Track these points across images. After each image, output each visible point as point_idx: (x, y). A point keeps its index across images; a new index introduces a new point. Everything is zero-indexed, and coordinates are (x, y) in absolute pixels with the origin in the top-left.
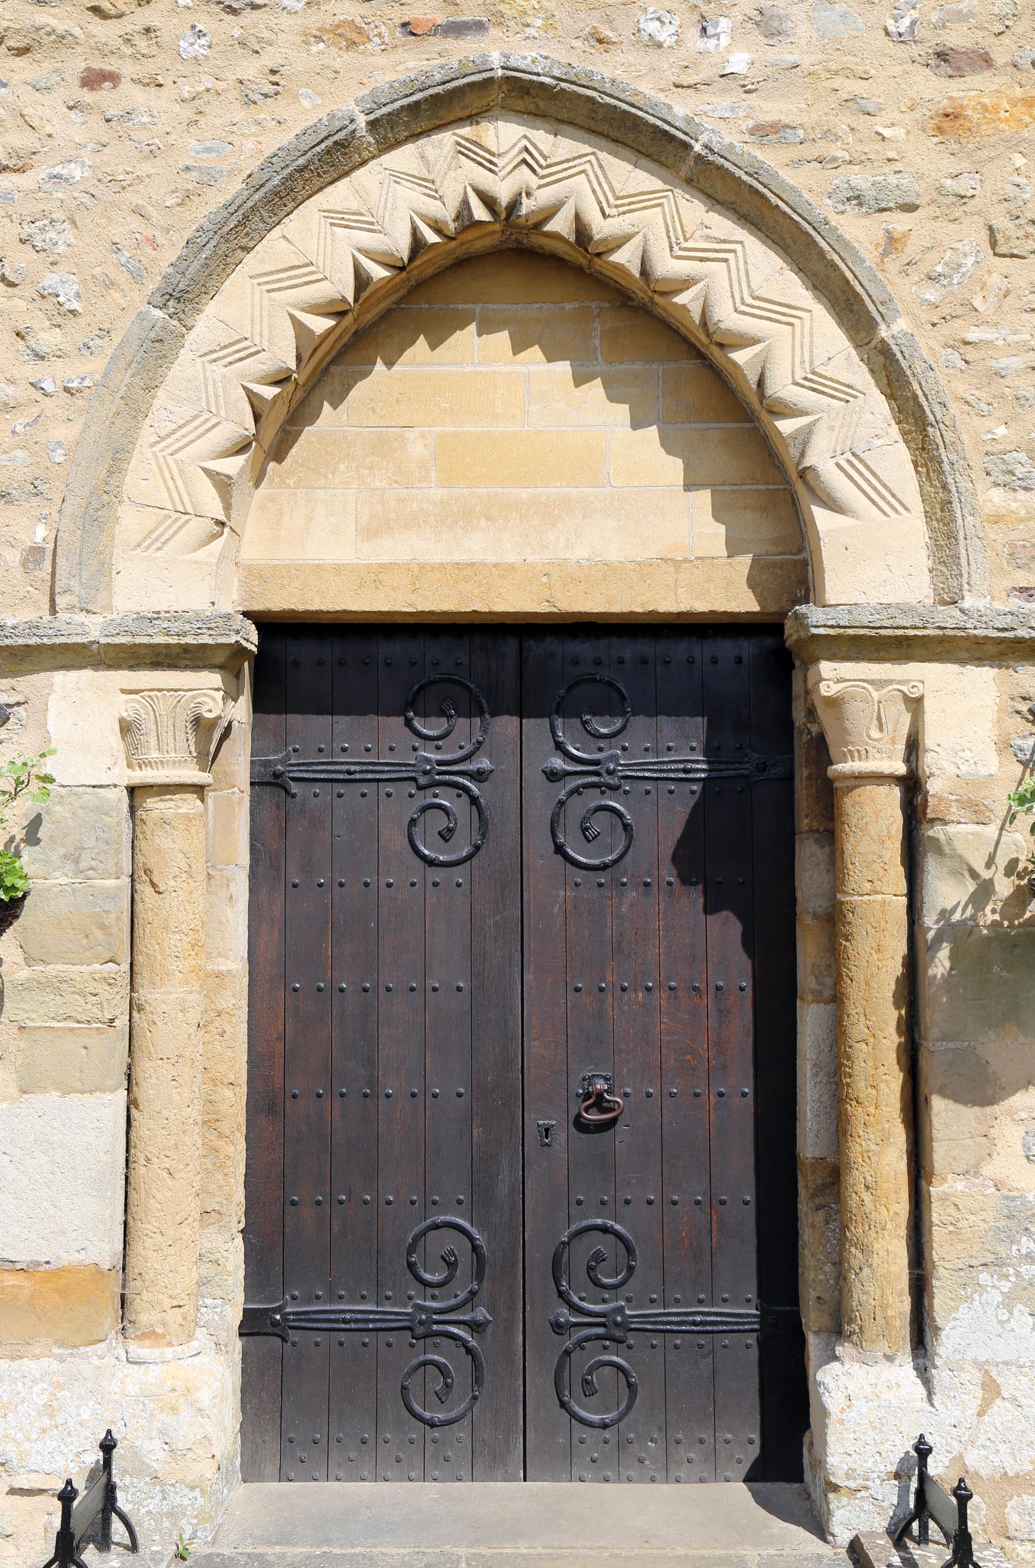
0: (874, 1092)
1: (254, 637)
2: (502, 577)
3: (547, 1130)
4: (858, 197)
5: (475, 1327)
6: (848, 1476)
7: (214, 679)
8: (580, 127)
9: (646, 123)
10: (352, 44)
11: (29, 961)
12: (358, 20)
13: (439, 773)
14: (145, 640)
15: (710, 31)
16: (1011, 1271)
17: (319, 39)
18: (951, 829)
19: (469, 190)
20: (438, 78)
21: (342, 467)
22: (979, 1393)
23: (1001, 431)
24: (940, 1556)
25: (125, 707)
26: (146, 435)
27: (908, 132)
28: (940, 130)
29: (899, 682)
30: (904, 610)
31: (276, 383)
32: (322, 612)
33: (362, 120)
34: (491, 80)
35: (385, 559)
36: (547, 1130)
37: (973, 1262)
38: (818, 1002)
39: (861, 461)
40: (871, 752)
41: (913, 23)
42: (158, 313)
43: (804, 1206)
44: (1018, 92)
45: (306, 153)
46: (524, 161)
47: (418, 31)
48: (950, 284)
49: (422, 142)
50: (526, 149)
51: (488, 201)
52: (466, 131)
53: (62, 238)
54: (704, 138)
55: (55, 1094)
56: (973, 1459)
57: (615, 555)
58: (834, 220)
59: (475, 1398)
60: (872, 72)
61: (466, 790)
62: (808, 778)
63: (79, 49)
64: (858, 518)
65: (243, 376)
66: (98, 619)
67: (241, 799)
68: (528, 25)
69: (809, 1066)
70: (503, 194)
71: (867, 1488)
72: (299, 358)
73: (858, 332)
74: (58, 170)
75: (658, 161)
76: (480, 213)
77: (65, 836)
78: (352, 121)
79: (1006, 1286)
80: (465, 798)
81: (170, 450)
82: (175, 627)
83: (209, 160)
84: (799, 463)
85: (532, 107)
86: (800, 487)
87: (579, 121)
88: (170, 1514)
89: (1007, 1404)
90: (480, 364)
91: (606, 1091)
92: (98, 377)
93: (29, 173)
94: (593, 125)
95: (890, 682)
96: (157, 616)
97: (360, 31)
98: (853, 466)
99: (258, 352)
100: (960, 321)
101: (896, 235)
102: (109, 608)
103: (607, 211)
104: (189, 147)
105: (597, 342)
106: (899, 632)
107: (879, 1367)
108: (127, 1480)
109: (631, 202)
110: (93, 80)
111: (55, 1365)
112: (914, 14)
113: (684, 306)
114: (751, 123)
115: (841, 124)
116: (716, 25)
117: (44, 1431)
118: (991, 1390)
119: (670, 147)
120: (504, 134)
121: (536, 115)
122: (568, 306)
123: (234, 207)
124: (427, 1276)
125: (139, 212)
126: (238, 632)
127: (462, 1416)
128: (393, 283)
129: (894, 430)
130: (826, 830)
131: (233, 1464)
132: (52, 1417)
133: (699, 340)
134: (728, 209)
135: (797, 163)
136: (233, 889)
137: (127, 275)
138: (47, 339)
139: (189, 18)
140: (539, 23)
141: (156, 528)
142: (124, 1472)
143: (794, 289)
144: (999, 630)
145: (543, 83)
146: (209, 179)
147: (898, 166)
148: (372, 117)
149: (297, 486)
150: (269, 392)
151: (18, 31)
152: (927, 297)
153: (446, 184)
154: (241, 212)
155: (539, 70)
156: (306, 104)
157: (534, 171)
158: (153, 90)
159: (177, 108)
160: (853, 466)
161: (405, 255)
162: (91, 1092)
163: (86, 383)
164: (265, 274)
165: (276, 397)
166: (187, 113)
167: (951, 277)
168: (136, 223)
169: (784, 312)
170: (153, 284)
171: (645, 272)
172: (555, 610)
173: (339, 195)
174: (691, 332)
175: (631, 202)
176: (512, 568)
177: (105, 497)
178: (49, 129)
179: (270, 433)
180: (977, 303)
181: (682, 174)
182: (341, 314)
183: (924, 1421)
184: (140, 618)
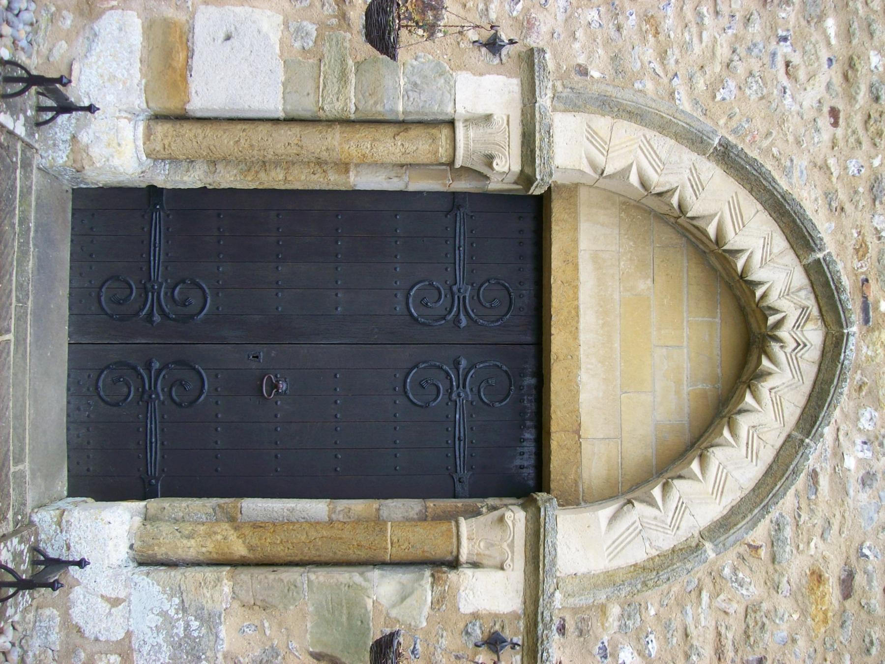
0: (278, 542)
1: (538, 192)
2: (571, 332)
3: (257, 357)
4: (779, 529)
5: (150, 314)
6: (67, 522)
7: (516, 167)
8: (817, 376)
9: (820, 412)
10: (857, 251)
11: (358, 65)
12: (869, 255)
13: (459, 297)
14: (537, 128)
15: (865, 446)
16: (180, 616)
17: (859, 233)
18: (428, 587)
19: (784, 314)
20: (843, 297)
21: (631, 243)
22: (113, 596)
23: (652, 612)
24: (25, 571)
25: (499, 117)
26: (650, 133)
27: (812, 556)
28: (813, 573)
29: (512, 557)
30: (553, 563)
31: (680, 206)
32: (550, 231)
33: (820, 255)
34: (842, 327)
35: (581, 267)
36: (257, 357)
37: (184, 595)
38: (329, 511)
39: (637, 535)
40: (472, 534)
41: (867, 557)
42: (716, 141)
43: (214, 501)
44: (830, 614)
45: (803, 224)
46: (799, 345)
47: (864, 288)
48: (732, 582)
49: (810, 289)
50: (805, 345)
51: (779, 324)
52: (815, 312)
53: (752, 93)
54: (812, 444)
55: (283, 78)
56: (78, 591)
57: (583, 397)
58: (768, 518)
59: (111, 316)
60: (843, 535)
61: (450, 312)
62: (456, 507)
63: (848, 107)
64: (606, 533)
65: (683, 187)
66: (548, 103)
67: (445, 185)
68: (868, 347)
69: (293, 505)
70: (783, 333)
71: (61, 532)
72: (693, 218)
73: (709, 532)
74: (788, 92)
75: (800, 419)
76: (772, 320)
77: (427, 84)
78: (820, 250)
79: (172, 612)
80: (445, 313)
81: (642, 146)
82: (545, 145)
83: (796, 174)
84: (636, 499)
85: (827, 349)
86: (622, 501)
87: (821, 376)
88: (54, 145)
89: (108, 611)
90: (688, 321)
91: (277, 391)
92: (681, 107)
93: (786, 77)
94: (818, 383)
95: (513, 552)
96: (550, 136)
97: (864, 256)
98: (635, 530)
99: (696, 195)
100: (712, 588)
101: (759, 551)
102: (554, 110)
103: (773, 391)
104: (802, 162)
105: (700, 387)
106: (541, 557)
107: (126, 540)
108: (74, 121)
109: (778, 404)
110: (834, 113)
111: (136, 81)
112: (871, 557)
113: (722, 434)
114: (818, 470)
115: (818, 521)
116: (868, 450)
117: (102, 76)
118: (115, 602)
119: (808, 426)
120: (814, 335)
121: (823, 351)
122: (719, 371)
123: (773, 184)
124: (178, 289)
125: (769, 134)
126: (542, 180)
127: (103, 309)
128: (733, 272)
129: (654, 553)
130: (427, 516)
131: (81, 182)
132: (109, 80)
133: (702, 443)
134: (775, 458)
135: (797, 495)
136: (395, 180)
137: (735, 126)
138: (701, 84)
139: (866, 165)
140: (869, 353)
141: (599, 137)
142: (78, 120)
143: (731, 498)
144: (543, 613)
145: (840, 355)
146: (787, 172)
147: (795, 552)
148: (822, 261)
149: (620, 218)
150: (675, 201)
151: (856, 76)
152: (726, 569)
153: (786, 301)
154: (771, 188)
155: (847, 353)
156: (827, 225)
157: (794, 350)
158: (830, 144)
159: (822, 157)
160: (635, 530)
161: (748, 278)
162: (284, 98)
163: (678, 102)
164: (738, 201)
165: (671, 205)
166: (819, 162)
167: (736, 582)
168: (763, 130)
169: (719, 490)
170: (732, 139)
171: (740, 412)
172: (552, 361)
173: (780, 242)
174: (706, 439)
175: (778, 404)
176: (576, 338)
177: (616, 109)
178: (809, 89)
179: (653, 203)
180: (722, 597)
181: (793, 433)
182: (717, 242)
183: (98, 565)
184: (550, 127)
